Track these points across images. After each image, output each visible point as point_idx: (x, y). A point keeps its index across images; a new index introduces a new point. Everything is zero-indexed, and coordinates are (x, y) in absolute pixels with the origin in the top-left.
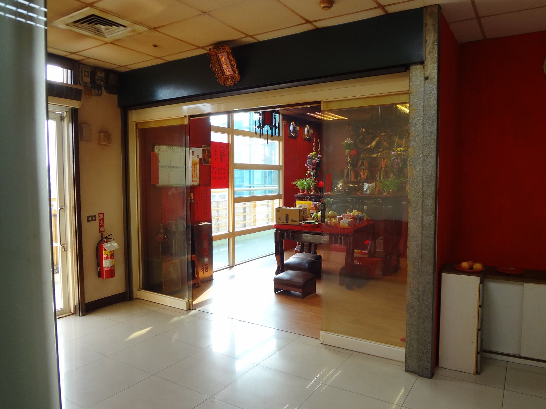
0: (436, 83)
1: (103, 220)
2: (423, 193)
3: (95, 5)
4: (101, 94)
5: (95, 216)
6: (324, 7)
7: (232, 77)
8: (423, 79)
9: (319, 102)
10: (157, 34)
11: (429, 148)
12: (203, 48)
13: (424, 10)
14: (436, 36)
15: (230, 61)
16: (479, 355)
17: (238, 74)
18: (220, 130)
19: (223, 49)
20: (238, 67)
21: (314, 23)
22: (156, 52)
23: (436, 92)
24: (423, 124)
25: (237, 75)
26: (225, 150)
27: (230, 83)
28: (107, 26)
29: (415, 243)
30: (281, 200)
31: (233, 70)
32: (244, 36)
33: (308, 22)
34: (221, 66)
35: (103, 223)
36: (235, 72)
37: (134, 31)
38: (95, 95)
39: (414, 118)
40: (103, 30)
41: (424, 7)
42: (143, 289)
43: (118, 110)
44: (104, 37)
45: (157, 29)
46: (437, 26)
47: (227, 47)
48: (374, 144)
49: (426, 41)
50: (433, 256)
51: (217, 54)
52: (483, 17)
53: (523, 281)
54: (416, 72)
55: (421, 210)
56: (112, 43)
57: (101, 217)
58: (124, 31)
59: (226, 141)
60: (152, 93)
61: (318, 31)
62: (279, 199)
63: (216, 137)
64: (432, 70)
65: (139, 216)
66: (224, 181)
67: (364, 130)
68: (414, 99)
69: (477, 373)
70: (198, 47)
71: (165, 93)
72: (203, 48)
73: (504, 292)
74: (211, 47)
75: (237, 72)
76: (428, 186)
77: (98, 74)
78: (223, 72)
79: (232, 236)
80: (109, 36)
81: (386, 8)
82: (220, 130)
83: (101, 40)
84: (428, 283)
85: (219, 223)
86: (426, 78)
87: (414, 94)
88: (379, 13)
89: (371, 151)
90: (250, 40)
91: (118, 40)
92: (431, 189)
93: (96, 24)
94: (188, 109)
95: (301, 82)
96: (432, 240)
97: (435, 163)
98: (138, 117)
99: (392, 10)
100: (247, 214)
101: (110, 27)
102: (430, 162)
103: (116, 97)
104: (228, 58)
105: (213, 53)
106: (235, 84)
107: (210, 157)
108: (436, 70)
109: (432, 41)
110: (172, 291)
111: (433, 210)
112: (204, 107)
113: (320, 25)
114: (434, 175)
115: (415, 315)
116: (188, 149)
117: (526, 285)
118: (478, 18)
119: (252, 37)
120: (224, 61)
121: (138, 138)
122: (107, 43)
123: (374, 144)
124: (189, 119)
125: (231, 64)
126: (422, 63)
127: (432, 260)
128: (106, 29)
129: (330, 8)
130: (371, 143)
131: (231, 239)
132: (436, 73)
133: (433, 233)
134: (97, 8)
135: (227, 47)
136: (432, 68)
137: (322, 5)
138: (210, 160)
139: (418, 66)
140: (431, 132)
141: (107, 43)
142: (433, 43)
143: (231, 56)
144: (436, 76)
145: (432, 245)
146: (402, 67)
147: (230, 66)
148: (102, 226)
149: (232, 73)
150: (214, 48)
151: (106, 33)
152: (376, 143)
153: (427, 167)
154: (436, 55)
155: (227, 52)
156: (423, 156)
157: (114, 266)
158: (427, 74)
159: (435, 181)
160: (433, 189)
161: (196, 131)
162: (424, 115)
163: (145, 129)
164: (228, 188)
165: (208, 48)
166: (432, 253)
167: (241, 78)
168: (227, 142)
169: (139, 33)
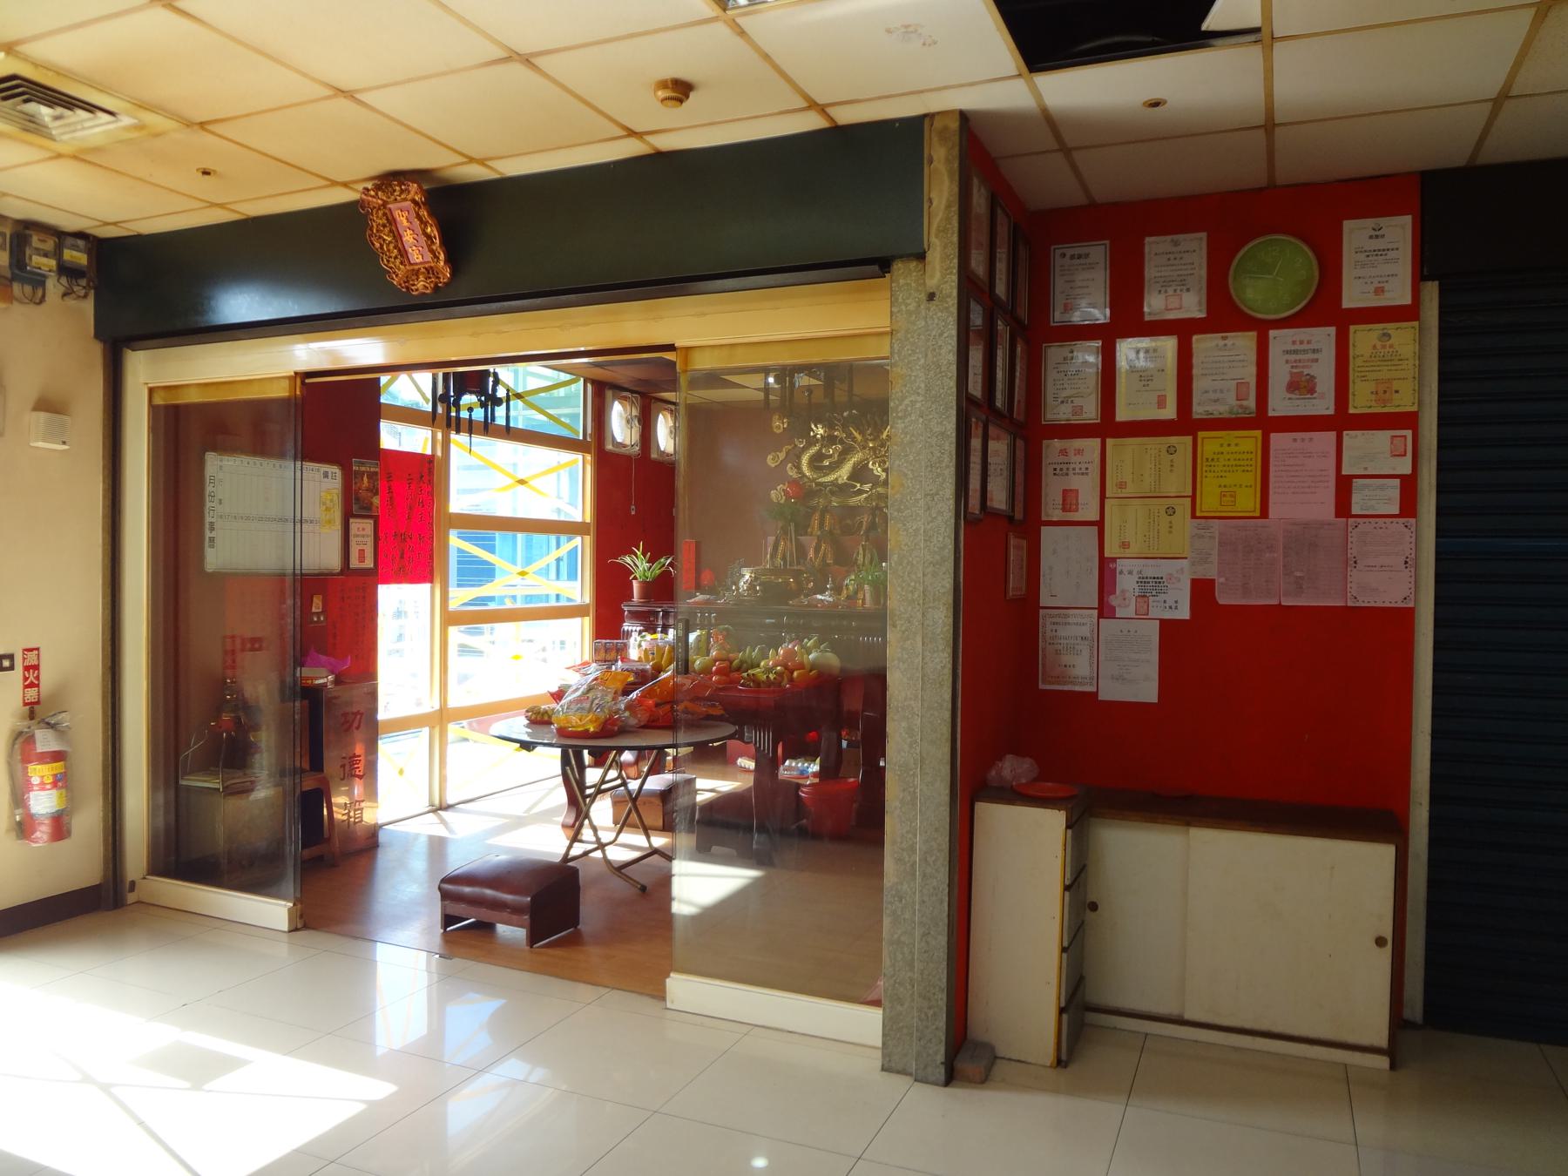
0: (954, 310)
1: (36, 667)
3: (19, 48)
4: (42, 300)
5: (11, 657)
6: (663, 100)
8: (923, 296)
11: (938, 475)
12: (345, 185)
13: (927, 122)
14: (956, 190)
15: (424, 223)
16: (1065, 1016)
18: (408, 415)
19: (402, 191)
20: (445, 243)
21: (649, 138)
22: (205, 187)
23: (954, 332)
26: (424, 475)
28: (59, 110)
31: (432, 251)
32: (460, 159)
33: (631, 133)
34: (398, 237)
35: (38, 678)
37: (140, 127)
38: (21, 302)
39: (903, 398)
40: (47, 119)
41: (925, 116)
43: (96, 351)
44: (52, 139)
45: (210, 127)
46: (956, 165)
47: (414, 187)
50: (947, 757)
51: (385, 204)
53: (1188, 824)
55: (919, 639)
56: (75, 157)
57: (32, 659)
58: (111, 127)
60: (199, 303)
61: (659, 156)
63: (395, 437)
64: (943, 276)
66: (417, 562)
67: (821, 431)
69: (1060, 1063)
70: (334, 183)
72: (345, 185)
73: (1140, 853)
74: (369, 185)
75: (442, 257)
76: (934, 574)
77: (35, 240)
78: (403, 253)
79: (440, 719)
80: (65, 137)
81: (832, 111)
82: (408, 415)
83: (41, 147)
86: (931, 297)
88: (811, 122)
89: (841, 489)
91: (97, 150)
92: (944, 583)
93: (26, 101)
95: (538, 301)
97: (952, 514)
98: (149, 371)
99: (847, 116)
101: (67, 112)
102: (940, 513)
103: (88, 306)
104: (419, 217)
106: (436, 288)
107: (376, 494)
108: (955, 278)
109: (944, 202)
111: (950, 635)
112: (360, 350)
114: (951, 547)
115: (907, 916)
118: (1066, 150)
119: (482, 162)
120: (405, 223)
121: (589, 468)
122: (59, 156)
124: (303, 383)
128: (57, 118)
129: (681, 101)
131: (437, 731)
132: (955, 284)
134: (25, 59)
135: (414, 187)
136: (941, 270)
137: (661, 94)
138: (376, 501)
139: (913, 265)
140: (942, 434)
141: (59, 156)
142: (948, 207)
143: (424, 213)
147: (423, 239)
148: (31, 685)
149: (429, 257)
150: (377, 188)
151: (55, 128)
152: (854, 467)
155: (414, 201)
158: (932, 282)
160: (948, 583)
161: (334, 418)
162: (928, 390)
163: (176, 407)
164: (431, 582)
165: (360, 187)
166: (947, 749)
168: (428, 452)
169: (157, 135)
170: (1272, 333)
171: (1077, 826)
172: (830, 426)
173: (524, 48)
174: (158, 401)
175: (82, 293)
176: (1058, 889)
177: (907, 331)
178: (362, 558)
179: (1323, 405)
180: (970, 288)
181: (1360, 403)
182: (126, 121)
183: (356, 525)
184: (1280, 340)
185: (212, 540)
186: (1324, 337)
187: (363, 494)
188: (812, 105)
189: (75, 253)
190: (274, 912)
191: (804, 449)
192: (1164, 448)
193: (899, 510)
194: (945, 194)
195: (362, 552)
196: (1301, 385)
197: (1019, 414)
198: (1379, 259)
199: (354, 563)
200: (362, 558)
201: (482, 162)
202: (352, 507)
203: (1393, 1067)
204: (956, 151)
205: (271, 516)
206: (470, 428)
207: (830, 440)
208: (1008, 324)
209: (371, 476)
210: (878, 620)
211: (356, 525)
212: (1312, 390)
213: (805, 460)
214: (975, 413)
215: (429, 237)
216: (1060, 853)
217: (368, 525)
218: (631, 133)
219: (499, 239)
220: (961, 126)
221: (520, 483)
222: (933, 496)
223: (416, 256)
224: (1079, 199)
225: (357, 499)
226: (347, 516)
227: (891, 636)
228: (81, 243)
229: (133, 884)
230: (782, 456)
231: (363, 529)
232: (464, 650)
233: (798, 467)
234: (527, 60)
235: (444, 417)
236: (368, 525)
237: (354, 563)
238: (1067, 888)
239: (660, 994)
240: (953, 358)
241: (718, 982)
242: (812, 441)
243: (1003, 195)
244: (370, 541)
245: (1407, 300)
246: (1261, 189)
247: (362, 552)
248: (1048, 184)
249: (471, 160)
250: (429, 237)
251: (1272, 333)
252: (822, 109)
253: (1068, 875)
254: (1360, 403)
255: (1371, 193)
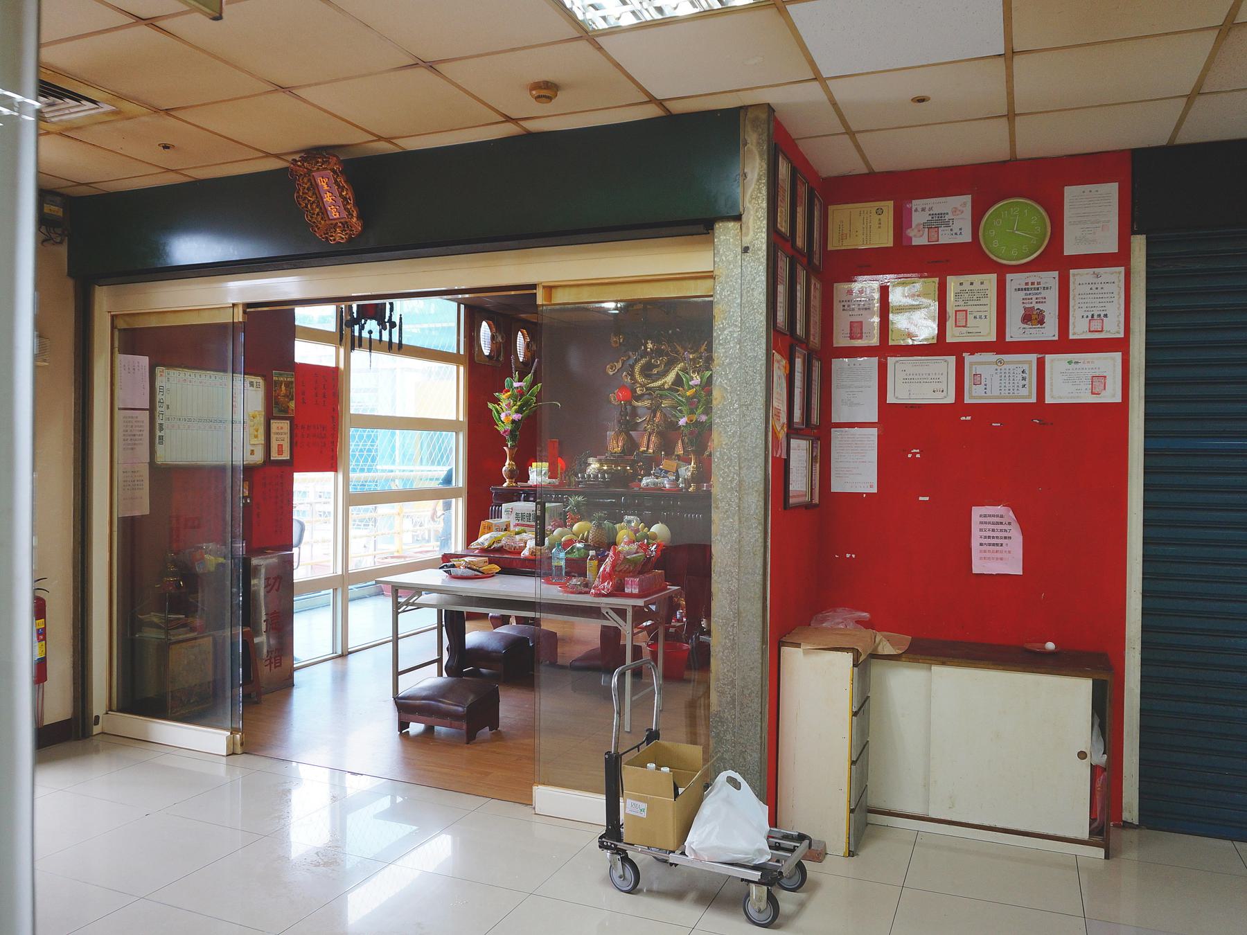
0: (764, 260)
2: (740, 482)
6: (539, 97)
7: (346, 225)
9: (534, 286)
10: (170, 122)
12: (277, 156)
13: (742, 114)
14: (765, 166)
15: (341, 188)
17: (358, 218)
20: (356, 204)
21: (521, 123)
23: (764, 278)
24: (740, 342)
25: (355, 220)
26: (327, 387)
27: (340, 236)
29: (726, 585)
30: (460, 500)
33: (509, 119)
36: (350, 214)
37: (116, 113)
39: (724, 329)
41: (741, 107)
42: (121, 710)
48: (670, 377)
49: (745, 175)
50: (760, 613)
52: (859, 132)
54: (726, 233)
55: (736, 518)
56: (61, 134)
59: (331, 363)
60: (159, 251)
61: (530, 136)
62: (456, 497)
63: (306, 353)
65: (115, 529)
68: (723, 290)
69: (851, 854)
70: (268, 155)
71: (190, 249)
72: (277, 156)
74: (297, 157)
78: (324, 212)
81: (667, 104)
84: (752, 669)
85: (312, 557)
86: (746, 250)
87: (722, 279)
88: (652, 112)
90: (384, 147)
94: (242, 290)
96: (759, 578)
99: (677, 108)
100: (380, 533)
103: (63, 250)
105: (302, 171)
106: (350, 240)
108: (764, 235)
110: (195, 709)
113: (533, 126)
114: (762, 446)
115: (728, 737)
116: (239, 378)
117: (935, 668)
118: (851, 133)
119: (388, 140)
120: (326, 187)
123: (670, 377)
124: (244, 312)
125: (341, 195)
126: (738, 218)
127: (760, 620)
130: (665, 373)
132: (764, 241)
133: (759, 563)
136: (755, 227)
138: (292, 405)
139: (731, 224)
143: (341, 180)
144: (764, 247)
145: (758, 590)
146: (697, 223)
149: (345, 214)
150: (303, 160)
153: (749, 428)
154: (764, 205)
155: (334, 172)
156: (740, 406)
157: (45, 659)
158: (747, 241)
159: (762, 457)
160: (759, 474)
164: (336, 471)
165: (290, 158)
167: (364, 227)
168: (333, 365)
170: (1009, 277)
171: (863, 664)
172: (656, 341)
173: (429, 57)
174: (121, 324)
175: (58, 240)
176: (848, 715)
177: (727, 276)
178: (280, 452)
179: (1049, 331)
180: (777, 241)
181: (1079, 330)
182: (107, 108)
183: (275, 425)
184: (1014, 281)
185: (161, 438)
186: (1050, 278)
187: (282, 399)
188: (652, 100)
189: (53, 208)
190: (210, 740)
191: (636, 361)
192: (874, 211)
193: (720, 417)
194: (757, 171)
195: (280, 446)
196: (1032, 317)
197: (815, 340)
198: (1093, 215)
199: (275, 456)
200: (280, 452)
201: (388, 140)
202: (273, 409)
203: (1107, 857)
204: (765, 137)
205: (219, 417)
206: (371, 346)
207: (658, 353)
208: (807, 268)
209: (288, 385)
210: (703, 502)
211: (275, 425)
212: (1041, 322)
213: (637, 369)
214: (783, 339)
215: (345, 199)
216: (848, 686)
217: (286, 425)
218: (509, 119)
219: (401, 202)
220: (769, 116)
221: (408, 391)
222: (747, 406)
223: (334, 214)
224: (862, 169)
225: (277, 403)
226: (269, 418)
227: (716, 516)
228: (58, 199)
229: (97, 717)
230: (619, 365)
231: (281, 428)
232: (365, 523)
233: (632, 375)
234: (431, 66)
235: (346, 338)
236: (286, 425)
237: (275, 456)
238: (855, 714)
239: (528, 801)
240: (763, 298)
241: (577, 792)
242: (645, 354)
243: (801, 168)
244: (287, 438)
245: (1113, 247)
246: (1005, 162)
247: (280, 446)
248: (836, 159)
249: (380, 138)
250: (345, 199)
251: (1009, 277)
252: (660, 103)
253: (855, 704)
254: (1079, 330)
255: (1089, 167)
